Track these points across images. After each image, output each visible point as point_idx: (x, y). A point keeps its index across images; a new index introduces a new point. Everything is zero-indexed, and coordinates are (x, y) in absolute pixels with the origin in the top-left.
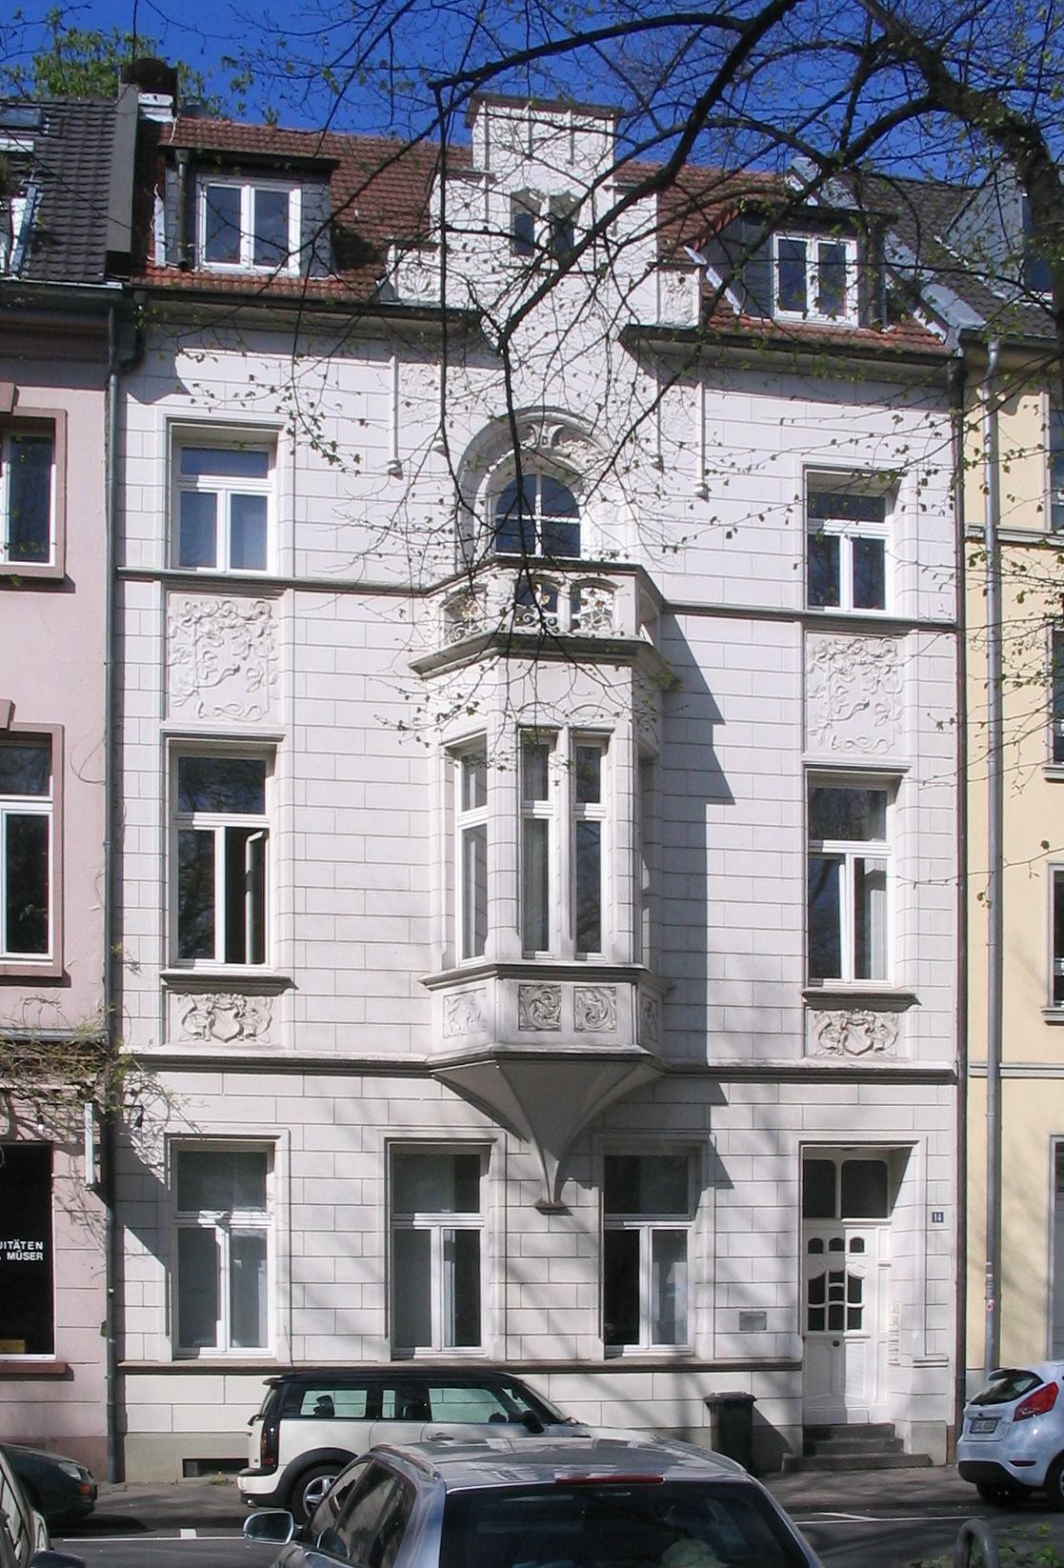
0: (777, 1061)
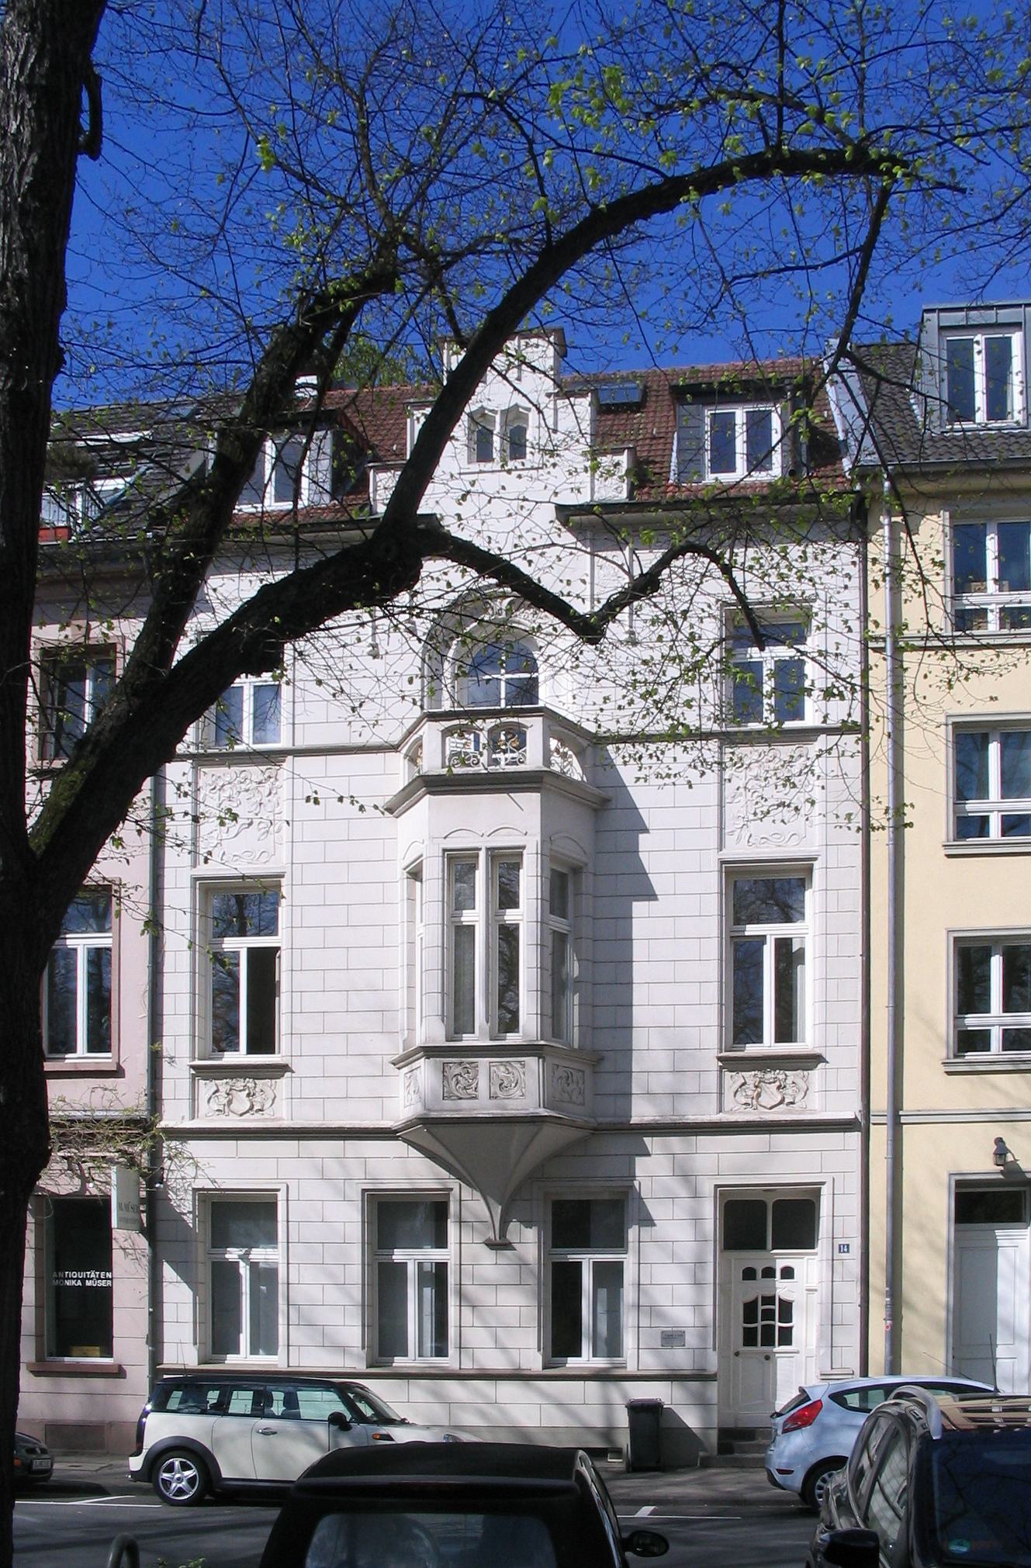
0: (692, 1117)
